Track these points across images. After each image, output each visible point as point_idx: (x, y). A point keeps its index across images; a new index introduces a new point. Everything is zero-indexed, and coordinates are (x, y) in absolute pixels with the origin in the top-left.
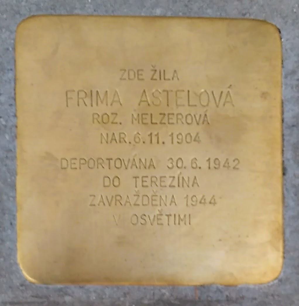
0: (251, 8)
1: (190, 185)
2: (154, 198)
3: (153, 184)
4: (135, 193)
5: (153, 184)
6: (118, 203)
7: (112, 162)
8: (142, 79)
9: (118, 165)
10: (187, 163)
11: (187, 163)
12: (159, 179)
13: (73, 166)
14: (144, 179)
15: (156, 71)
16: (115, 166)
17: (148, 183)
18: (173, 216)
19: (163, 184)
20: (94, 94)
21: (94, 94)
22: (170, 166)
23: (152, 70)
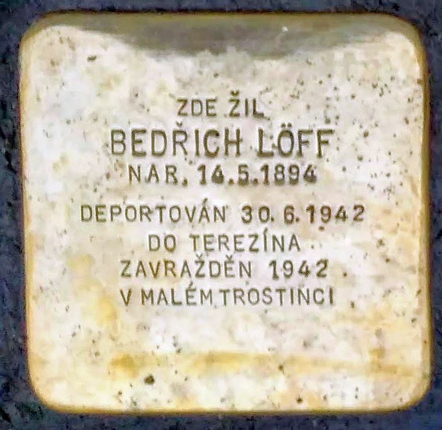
0: (125, 71)
1: (286, 246)
3: (223, 247)
4: (196, 259)
5: (223, 247)
6: (169, 272)
7: (166, 213)
8: (214, 115)
9: (175, 215)
10: (278, 212)
11: (278, 212)
14: (138, 137)
15: (238, 101)
16: (172, 219)
17: (146, 147)
18: (289, 292)
19: (238, 246)
20: (296, 293)
21: (296, 293)
22: (247, 218)
23: (232, 101)
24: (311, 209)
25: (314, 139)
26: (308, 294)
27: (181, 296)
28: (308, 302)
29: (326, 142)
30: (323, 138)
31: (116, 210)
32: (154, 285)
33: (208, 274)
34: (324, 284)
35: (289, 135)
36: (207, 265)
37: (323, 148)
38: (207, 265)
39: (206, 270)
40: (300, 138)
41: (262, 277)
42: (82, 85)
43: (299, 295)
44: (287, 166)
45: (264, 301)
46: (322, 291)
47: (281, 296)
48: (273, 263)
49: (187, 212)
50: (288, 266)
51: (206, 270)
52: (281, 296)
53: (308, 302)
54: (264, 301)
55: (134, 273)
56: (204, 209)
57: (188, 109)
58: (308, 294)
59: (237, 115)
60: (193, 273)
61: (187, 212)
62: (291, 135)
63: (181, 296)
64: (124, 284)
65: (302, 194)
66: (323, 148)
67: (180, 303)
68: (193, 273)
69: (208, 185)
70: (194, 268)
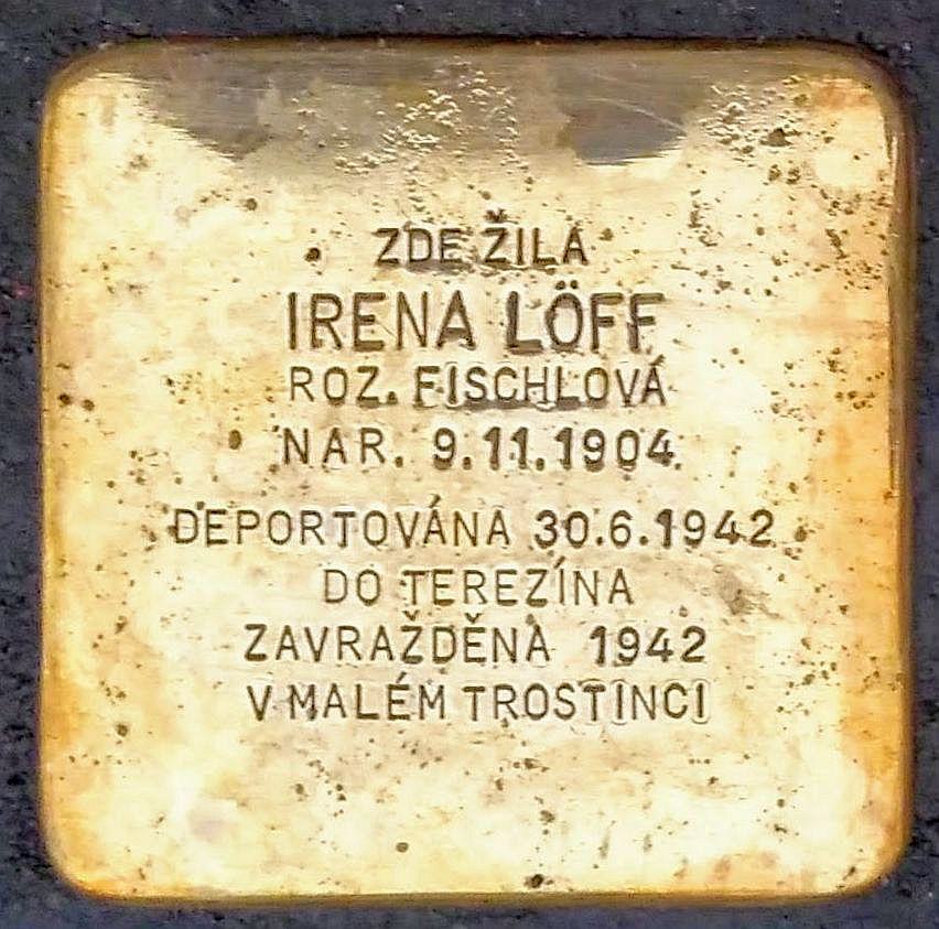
2: (473, 638)
12: (348, 307)
13: (473, 653)
18: (612, 690)
24: (665, 517)
25: (621, 313)
26: (634, 707)
27: (375, 703)
28: (652, 716)
29: (650, 320)
30: (643, 311)
31: (248, 520)
32: (320, 675)
33: (428, 657)
34: (688, 674)
35: (571, 304)
36: (427, 636)
37: (643, 330)
38: (427, 636)
39: (423, 648)
40: (594, 311)
41: (570, 656)
42: (141, 189)
43: (631, 700)
44: (319, 372)
45: (557, 712)
46: (684, 692)
47: (595, 700)
48: (600, 632)
49: (400, 524)
50: (630, 639)
51: (423, 648)
52: (595, 700)
53: (652, 716)
54: (557, 712)
55: (272, 655)
56: (435, 515)
57: (400, 251)
58: (634, 707)
59: (502, 262)
60: (397, 652)
61: (400, 524)
62: (577, 304)
63: (375, 703)
64: (258, 677)
65: (654, 486)
66: (643, 330)
67: (374, 716)
68: (397, 652)
69: (670, 467)
70: (398, 642)
